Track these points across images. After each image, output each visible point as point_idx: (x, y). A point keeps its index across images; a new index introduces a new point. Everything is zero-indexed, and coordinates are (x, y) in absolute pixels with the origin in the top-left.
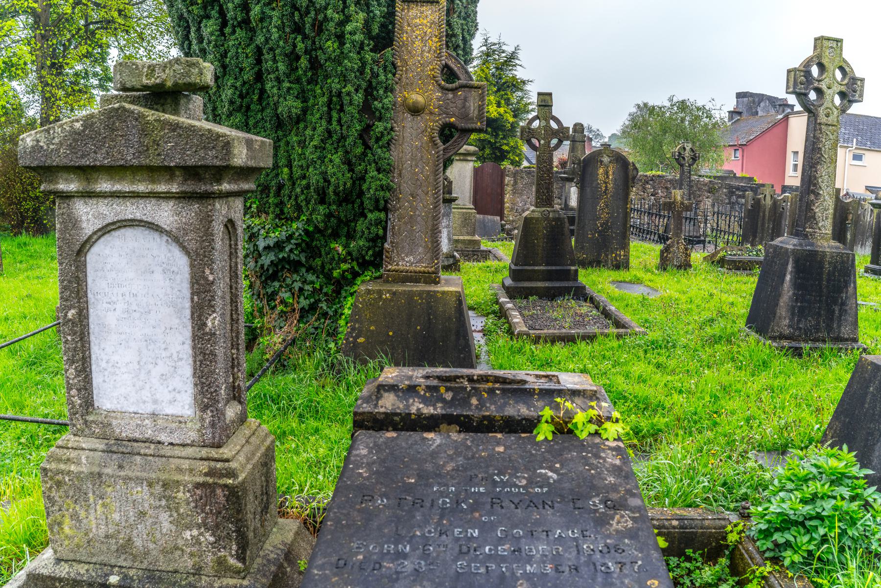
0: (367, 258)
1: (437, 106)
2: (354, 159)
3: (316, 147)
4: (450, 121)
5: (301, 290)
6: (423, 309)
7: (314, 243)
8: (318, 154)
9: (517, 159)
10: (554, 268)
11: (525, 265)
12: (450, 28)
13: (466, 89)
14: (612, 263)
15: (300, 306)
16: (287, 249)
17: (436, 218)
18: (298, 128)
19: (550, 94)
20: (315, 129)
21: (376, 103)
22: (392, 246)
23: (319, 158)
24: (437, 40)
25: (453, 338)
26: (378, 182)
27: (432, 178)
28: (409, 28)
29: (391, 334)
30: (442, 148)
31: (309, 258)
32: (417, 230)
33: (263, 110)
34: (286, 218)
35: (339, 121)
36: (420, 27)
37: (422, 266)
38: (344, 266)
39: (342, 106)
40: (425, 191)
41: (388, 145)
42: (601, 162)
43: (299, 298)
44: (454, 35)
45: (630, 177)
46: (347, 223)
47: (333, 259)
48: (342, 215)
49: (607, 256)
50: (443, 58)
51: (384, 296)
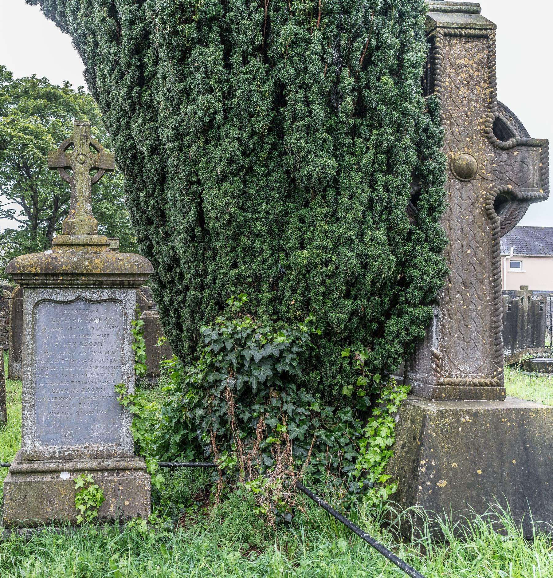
1: (489, 170)
6: (515, 435)
13: (523, 148)
22: (442, 351)
24: (486, 85)
28: (452, 70)
29: (479, 472)
32: (473, 330)
33: (268, 174)
36: (466, 69)
37: (481, 377)
40: (481, 279)
51: (463, 420)
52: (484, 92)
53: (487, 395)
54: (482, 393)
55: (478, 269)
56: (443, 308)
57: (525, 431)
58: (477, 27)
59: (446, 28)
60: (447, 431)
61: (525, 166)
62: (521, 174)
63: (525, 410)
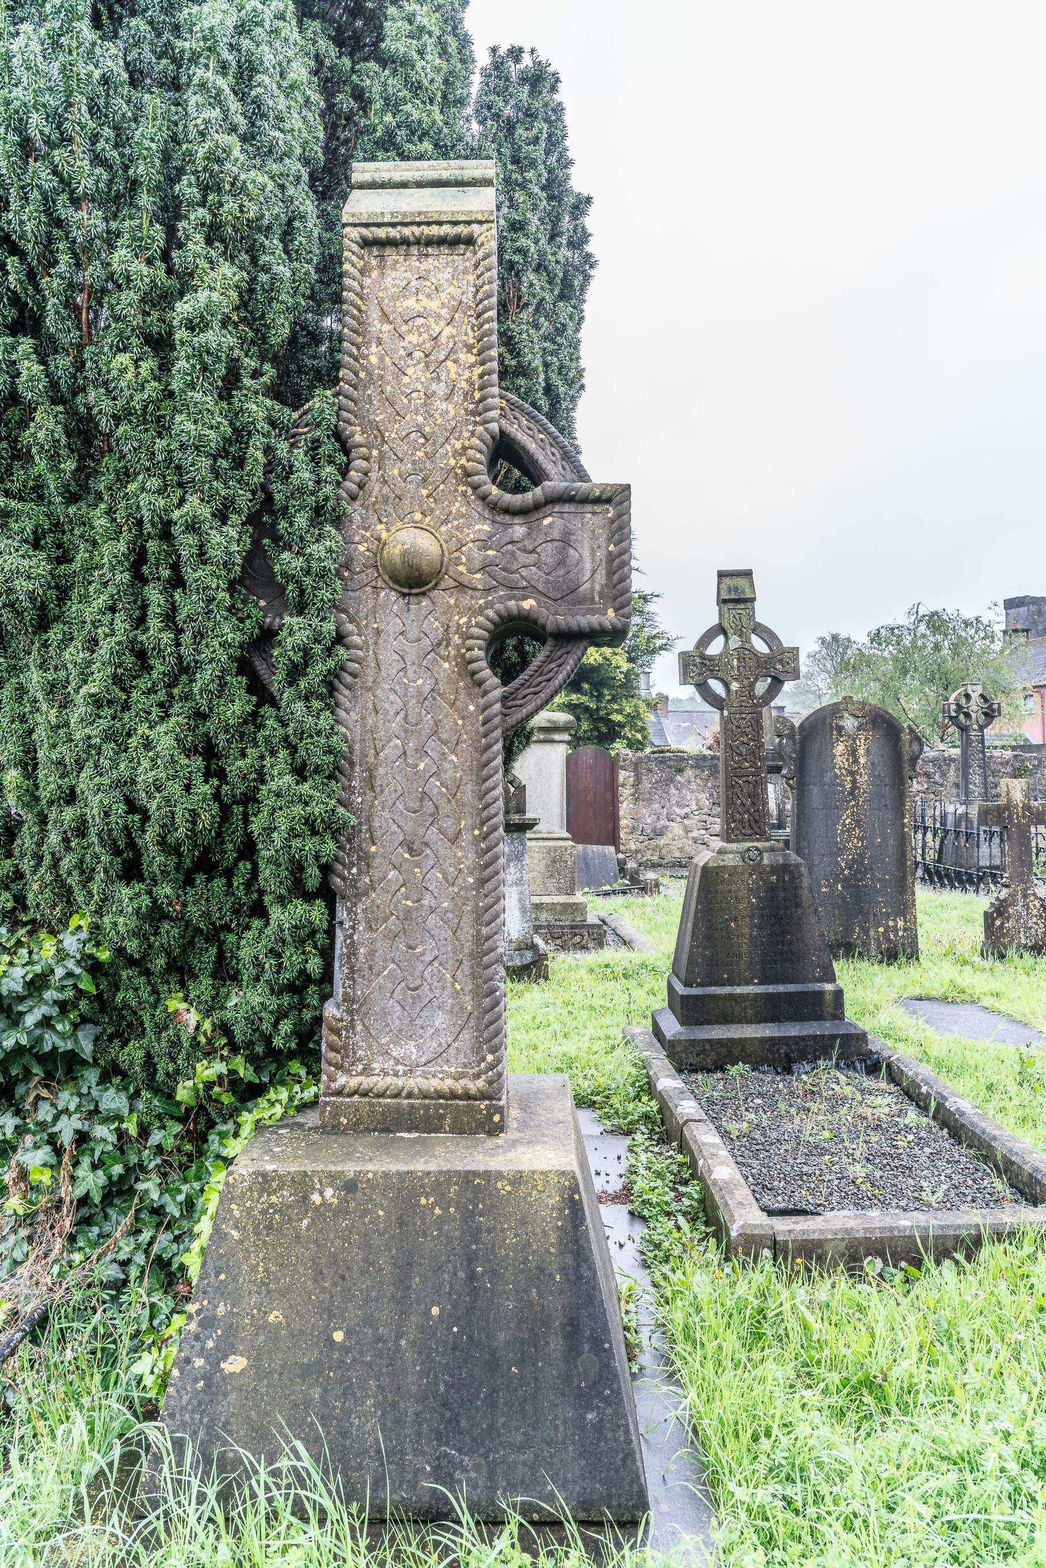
0: (278, 1042)
1: (478, 566)
2: (222, 737)
3: (97, 702)
4: (520, 609)
5: (82, 1138)
6: (449, 1240)
7: (119, 997)
8: (104, 724)
9: (639, 736)
10: (781, 988)
11: (711, 984)
12: (511, 352)
13: (567, 508)
14: (879, 947)
15: (79, 1192)
16: (30, 1020)
17: (487, 917)
18: (45, 645)
19: (748, 574)
20: (96, 642)
21: (286, 555)
23: (109, 736)
24: (472, 359)
25: (556, 1345)
26: (298, 810)
27: (469, 789)
28: (386, 327)
29: (338, 1336)
30: (498, 693)
31: (110, 1040)
32: (428, 958)
34: (33, 921)
35: (170, 617)
36: (420, 321)
37: (450, 1076)
38: (208, 1070)
39: (175, 567)
41: (331, 683)
42: (840, 729)
43: (76, 1164)
44: (523, 371)
45: (906, 758)
46: (215, 934)
47: (175, 1043)
48: (194, 912)
49: (866, 932)
50: (494, 413)
51: (316, 1198)
52: (467, 374)
53: (454, 1122)
54: (443, 1117)
55: (446, 808)
56: (355, 905)
57: (479, 1229)
58: (444, 218)
59: (366, 225)
60: (269, 1227)
61: (572, 552)
62: (562, 572)
63: (487, 1175)
